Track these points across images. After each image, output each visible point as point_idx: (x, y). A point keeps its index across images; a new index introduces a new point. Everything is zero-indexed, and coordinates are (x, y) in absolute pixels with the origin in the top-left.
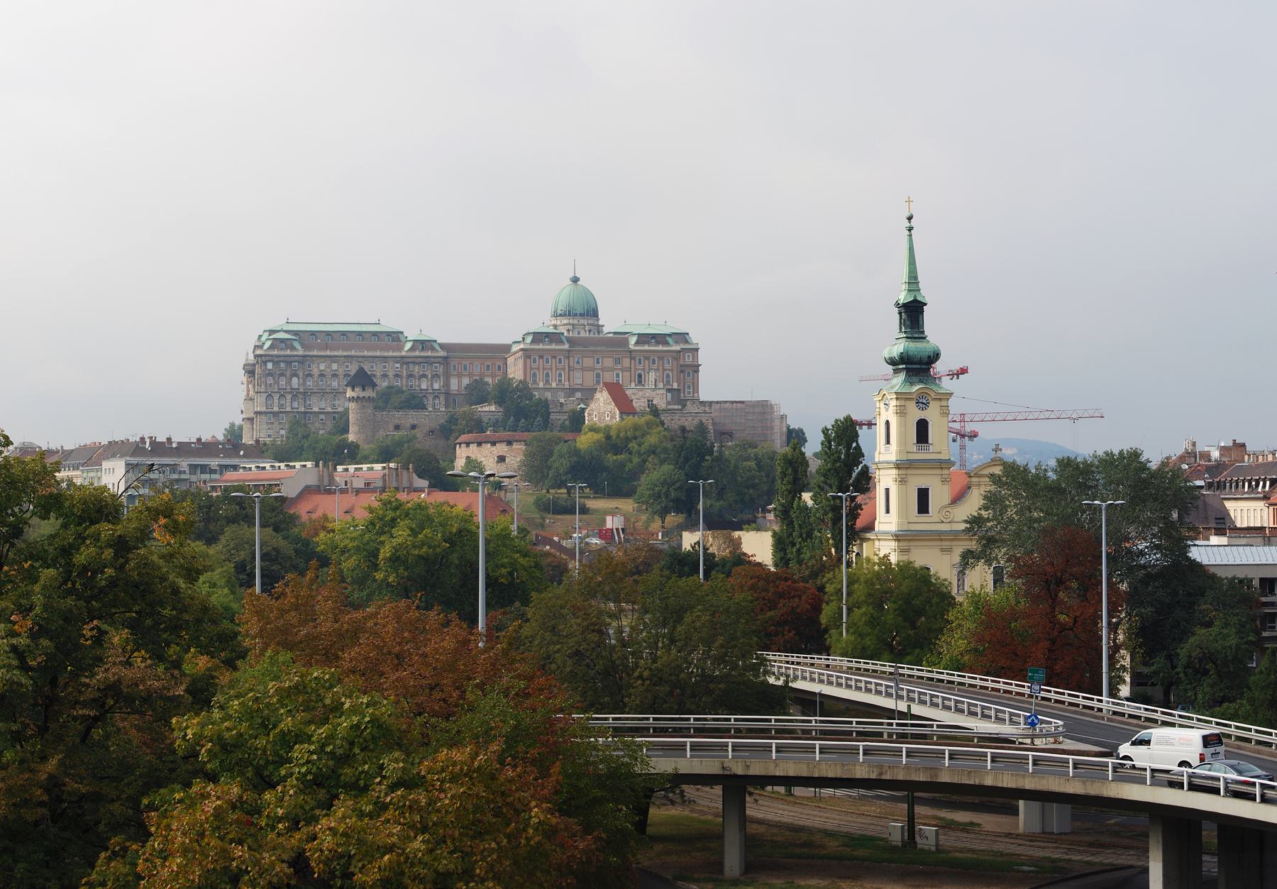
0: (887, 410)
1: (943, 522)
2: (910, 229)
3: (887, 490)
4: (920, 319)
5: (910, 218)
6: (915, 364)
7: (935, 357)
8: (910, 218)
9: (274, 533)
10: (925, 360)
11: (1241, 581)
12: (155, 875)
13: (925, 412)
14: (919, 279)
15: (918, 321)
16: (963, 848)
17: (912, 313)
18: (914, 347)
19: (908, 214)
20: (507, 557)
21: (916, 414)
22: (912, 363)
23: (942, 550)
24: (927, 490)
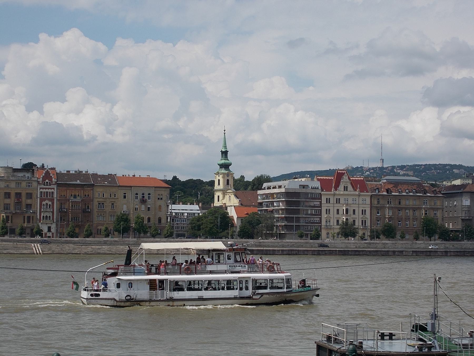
2: (225, 133)
3: (218, 196)
7: (230, 164)
8: (225, 131)
17: (225, 154)
18: (227, 161)
19: (224, 130)
21: (227, 178)
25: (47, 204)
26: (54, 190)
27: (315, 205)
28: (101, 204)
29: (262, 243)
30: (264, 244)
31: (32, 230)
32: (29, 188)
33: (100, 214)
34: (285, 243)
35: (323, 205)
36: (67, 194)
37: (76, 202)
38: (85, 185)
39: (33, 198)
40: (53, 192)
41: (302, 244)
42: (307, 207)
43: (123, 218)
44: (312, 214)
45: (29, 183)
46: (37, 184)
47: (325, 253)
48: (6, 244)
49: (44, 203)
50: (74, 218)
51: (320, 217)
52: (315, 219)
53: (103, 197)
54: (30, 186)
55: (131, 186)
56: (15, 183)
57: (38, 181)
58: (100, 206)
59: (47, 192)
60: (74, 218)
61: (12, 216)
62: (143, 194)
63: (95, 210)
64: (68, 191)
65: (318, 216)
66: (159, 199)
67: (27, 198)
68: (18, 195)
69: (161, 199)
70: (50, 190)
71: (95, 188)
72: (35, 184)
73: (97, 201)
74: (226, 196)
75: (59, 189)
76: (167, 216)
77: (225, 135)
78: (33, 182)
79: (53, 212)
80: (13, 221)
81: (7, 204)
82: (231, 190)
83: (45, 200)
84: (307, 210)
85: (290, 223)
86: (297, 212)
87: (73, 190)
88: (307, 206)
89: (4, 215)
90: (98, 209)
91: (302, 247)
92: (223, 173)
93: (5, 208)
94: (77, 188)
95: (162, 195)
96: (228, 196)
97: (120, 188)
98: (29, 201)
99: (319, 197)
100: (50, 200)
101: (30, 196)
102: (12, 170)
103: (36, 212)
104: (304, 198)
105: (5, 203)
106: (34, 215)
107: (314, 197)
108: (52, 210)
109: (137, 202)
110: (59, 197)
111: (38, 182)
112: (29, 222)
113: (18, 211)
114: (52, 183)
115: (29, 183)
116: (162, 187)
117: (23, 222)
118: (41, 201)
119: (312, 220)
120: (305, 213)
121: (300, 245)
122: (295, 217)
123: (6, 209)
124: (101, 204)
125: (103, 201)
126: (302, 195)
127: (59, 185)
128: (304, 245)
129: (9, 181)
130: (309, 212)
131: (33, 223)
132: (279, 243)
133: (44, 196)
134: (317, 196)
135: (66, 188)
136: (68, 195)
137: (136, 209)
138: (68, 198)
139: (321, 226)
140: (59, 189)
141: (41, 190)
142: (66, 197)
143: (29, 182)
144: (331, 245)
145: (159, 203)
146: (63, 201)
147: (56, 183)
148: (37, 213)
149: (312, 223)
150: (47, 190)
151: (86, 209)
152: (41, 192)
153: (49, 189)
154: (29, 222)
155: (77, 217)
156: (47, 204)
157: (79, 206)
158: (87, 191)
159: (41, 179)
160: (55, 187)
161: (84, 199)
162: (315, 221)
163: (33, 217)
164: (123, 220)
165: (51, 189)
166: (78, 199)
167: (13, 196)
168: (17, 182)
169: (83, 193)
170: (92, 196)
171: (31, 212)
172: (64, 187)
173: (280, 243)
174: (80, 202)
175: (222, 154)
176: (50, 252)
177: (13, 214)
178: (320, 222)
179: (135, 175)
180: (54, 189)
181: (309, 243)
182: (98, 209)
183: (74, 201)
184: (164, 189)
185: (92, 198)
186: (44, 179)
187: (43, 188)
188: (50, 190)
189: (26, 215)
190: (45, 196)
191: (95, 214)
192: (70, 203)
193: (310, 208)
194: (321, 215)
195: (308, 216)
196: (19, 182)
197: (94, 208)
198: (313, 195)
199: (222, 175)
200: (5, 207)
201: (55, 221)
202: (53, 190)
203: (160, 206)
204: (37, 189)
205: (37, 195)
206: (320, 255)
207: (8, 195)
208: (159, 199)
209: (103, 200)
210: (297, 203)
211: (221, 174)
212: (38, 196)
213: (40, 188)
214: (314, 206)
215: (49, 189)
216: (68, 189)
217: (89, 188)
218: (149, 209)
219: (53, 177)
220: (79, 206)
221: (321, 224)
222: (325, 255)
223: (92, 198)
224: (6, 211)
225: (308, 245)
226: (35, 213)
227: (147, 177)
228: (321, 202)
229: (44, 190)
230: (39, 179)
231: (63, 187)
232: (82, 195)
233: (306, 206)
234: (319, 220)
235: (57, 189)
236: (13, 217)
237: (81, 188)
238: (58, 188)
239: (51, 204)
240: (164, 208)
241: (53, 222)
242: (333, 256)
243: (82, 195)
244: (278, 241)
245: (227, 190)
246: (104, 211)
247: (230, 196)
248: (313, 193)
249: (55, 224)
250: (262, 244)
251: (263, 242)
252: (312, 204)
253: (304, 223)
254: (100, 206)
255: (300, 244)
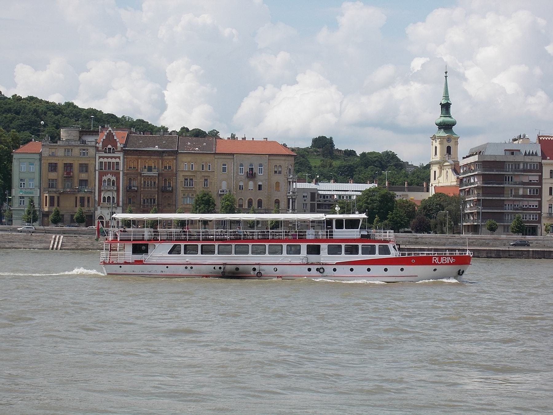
0: (436, 142)
2: (446, 77)
3: (435, 172)
7: (454, 124)
8: (446, 73)
9: (278, 181)
11: (213, 203)
12: (440, 205)
17: (446, 107)
18: (448, 119)
19: (445, 71)
21: (446, 144)
25: (109, 180)
26: (119, 158)
27: (531, 181)
28: (189, 181)
29: (419, 239)
30: (423, 240)
31: (72, 216)
32: (84, 156)
33: (186, 194)
34: (458, 239)
35: (544, 181)
36: (138, 165)
37: (150, 176)
38: (163, 152)
39: (89, 170)
40: (118, 163)
41: (487, 241)
42: (516, 185)
43: (203, 200)
44: (523, 196)
45: (84, 150)
46: (95, 151)
47: (509, 255)
48: (16, 235)
49: (105, 178)
50: (148, 200)
51: (538, 199)
52: (531, 203)
53: (192, 169)
54: (86, 154)
55: (232, 154)
56: (64, 150)
57: (96, 147)
58: (187, 183)
59: (105, 163)
60: (148, 200)
61: (58, 198)
62: (251, 165)
63: (180, 188)
64: (139, 161)
65: (535, 199)
66: (276, 172)
67: (81, 171)
68: (68, 167)
69: (280, 173)
70: (114, 160)
71: (180, 157)
72: (92, 151)
73: (183, 176)
74: (443, 171)
75: (127, 158)
76: (289, 197)
77: (446, 79)
78: (89, 148)
79: (118, 191)
80: (61, 204)
81: (53, 180)
82: (448, 162)
83: (106, 174)
84: (518, 189)
85: (491, 209)
86: (501, 192)
87: (147, 159)
88: (516, 182)
89: (47, 195)
90: (183, 187)
91: (488, 244)
92: (440, 137)
93: (49, 185)
94: (152, 157)
95: (280, 166)
96: (445, 171)
97: (216, 156)
98: (84, 176)
99: (539, 168)
100: (113, 174)
101: (84, 168)
102: (78, 132)
103: (93, 191)
104: (512, 170)
105: (49, 178)
106: (90, 195)
107: (529, 168)
108: (115, 188)
109: (242, 177)
110: (127, 170)
111: (97, 148)
112: (82, 205)
113: (68, 190)
114: (117, 149)
115: (84, 150)
116: (281, 155)
117: (75, 206)
118: (101, 175)
119: (525, 204)
120: (513, 193)
121: (484, 242)
122: (482, 199)
123: (51, 187)
124: (189, 180)
125: (192, 176)
126: (509, 165)
127: (126, 152)
128: (491, 244)
129: (55, 147)
130: (521, 192)
131: (88, 206)
132: (448, 238)
133: (105, 169)
134: (534, 167)
135: (136, 157)
136: (139, 166)
137: (241, 188)
138: (139, 171)
139: (540, 215)
140: (127, 158)
141: (101, 160)
142: (137, 170)
143: (84, 148)
144: (537, 243)
145: (276, 178)
146: (132, 176)
147: (123, 150)
148: (95, 193)
149: (524, 209)
150: (110, 160)
151: (165, 187)
152: (101, 163)
153: (112, 158)
154: (82, 205)
155: (151, 200)
156: (109, 180)
157: (155, 183)
158: (168, 162)
159: (101, 144)
160: (121, 155)
161: (163, 172)
162: (530, 206)
163: (89, 198)
164: (204, 202)
165: (115, 158)
166: (154, 173)
167: (60, 167)
168: (66, 148)
169: (162, 164)
170: (175, 168)
171: (85, 192)
172: (135, 155)
173: (449, 240)
174: (156, 176)
175: (442, 107)
176: (73, 247)
177: (60, 194)
178: (540, 207)
179: (245, 138)
180: (119, 158)
181: (499, 239)
182: (183, 187)
183: (146, 176)
184: (283, 158)
185: (174, 171)
186: (105, 143)
187: (103, 157)
188: (114, 160)
189: (79, 196)
190: (106, 168)
191: (180, 194)
192: (142, 179)
193: (522, 186)
194: (541, 196)
195: (517, 199)
196: (69, 148)
197: (179, 185)
198: (527, 166)
199: (439, 140)
200: (49, 183)
201: (121, 204)
202: (118, 160)
203: (278, 184)
204: (95, 158)
205: (95, 167)
206: (500, 258)
207: (53, 167)
208: (276, 172)
209: (192, 175)
210: (501, 179)
211: (438, 139)
212: (97, 168)
213: (100, 157)
214: (530, 183)
215: (112, 158)
216: (139, 158)
217: (170, 157)
218: (260, 187)
219: (117, 140)
220: (155, 183)
221: (541, 210)
222: (509, 258)
223: (174, 171)
224: (50, 189)
225: (498, 243)
226: (92, 192)
227: (263, 140)
228: (541, 177)
229: (106, 160)
230: (98, 144)
231: (132, 155)
232: (160, 167)
233: (516, 183)
234: (537, 205)
235: (124, 158)
236: (60, 198)
237: (159, 157)
238: (125, 156)
239: (115, 180)
240: (283, 186)
241: (118, 205)
242: (524, 260)
243: (160, 167)
244: (447, 236)
245: (444, 163)
246: (194, 189)
247: (447, 171)
248: (527, 163)
249: (121, 208)
250: (419, 240)
251: (422, 238)
252: (526, 180)
253: (511, 209)
254: (187, 183)
255: (484, 241)
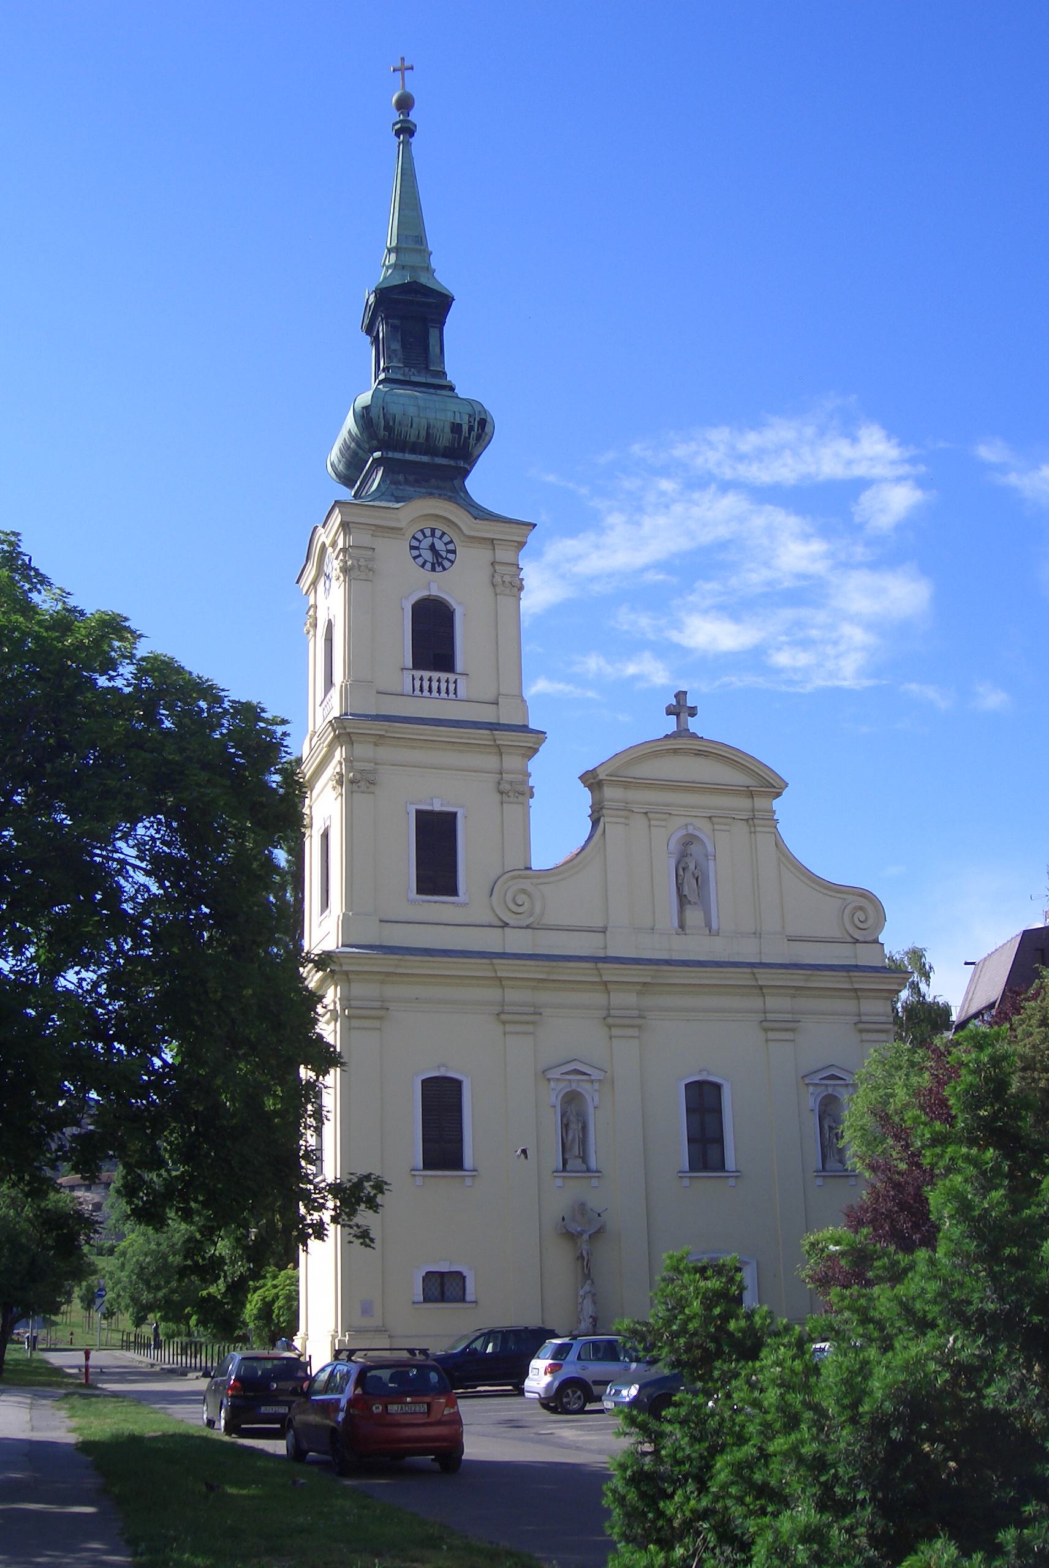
1: (506, 925)
4: (433, 341)
5: (403, 69)
6: (414, 449)
10: (445, 438)
13: (439, 575)
14: (432, 244)
15: (426, 348)
16: (838, 1121)
19: (402, 56)
20: (963, 1346)
22: (402, 445)
23: (502, 1014)
24: (450, 819)
